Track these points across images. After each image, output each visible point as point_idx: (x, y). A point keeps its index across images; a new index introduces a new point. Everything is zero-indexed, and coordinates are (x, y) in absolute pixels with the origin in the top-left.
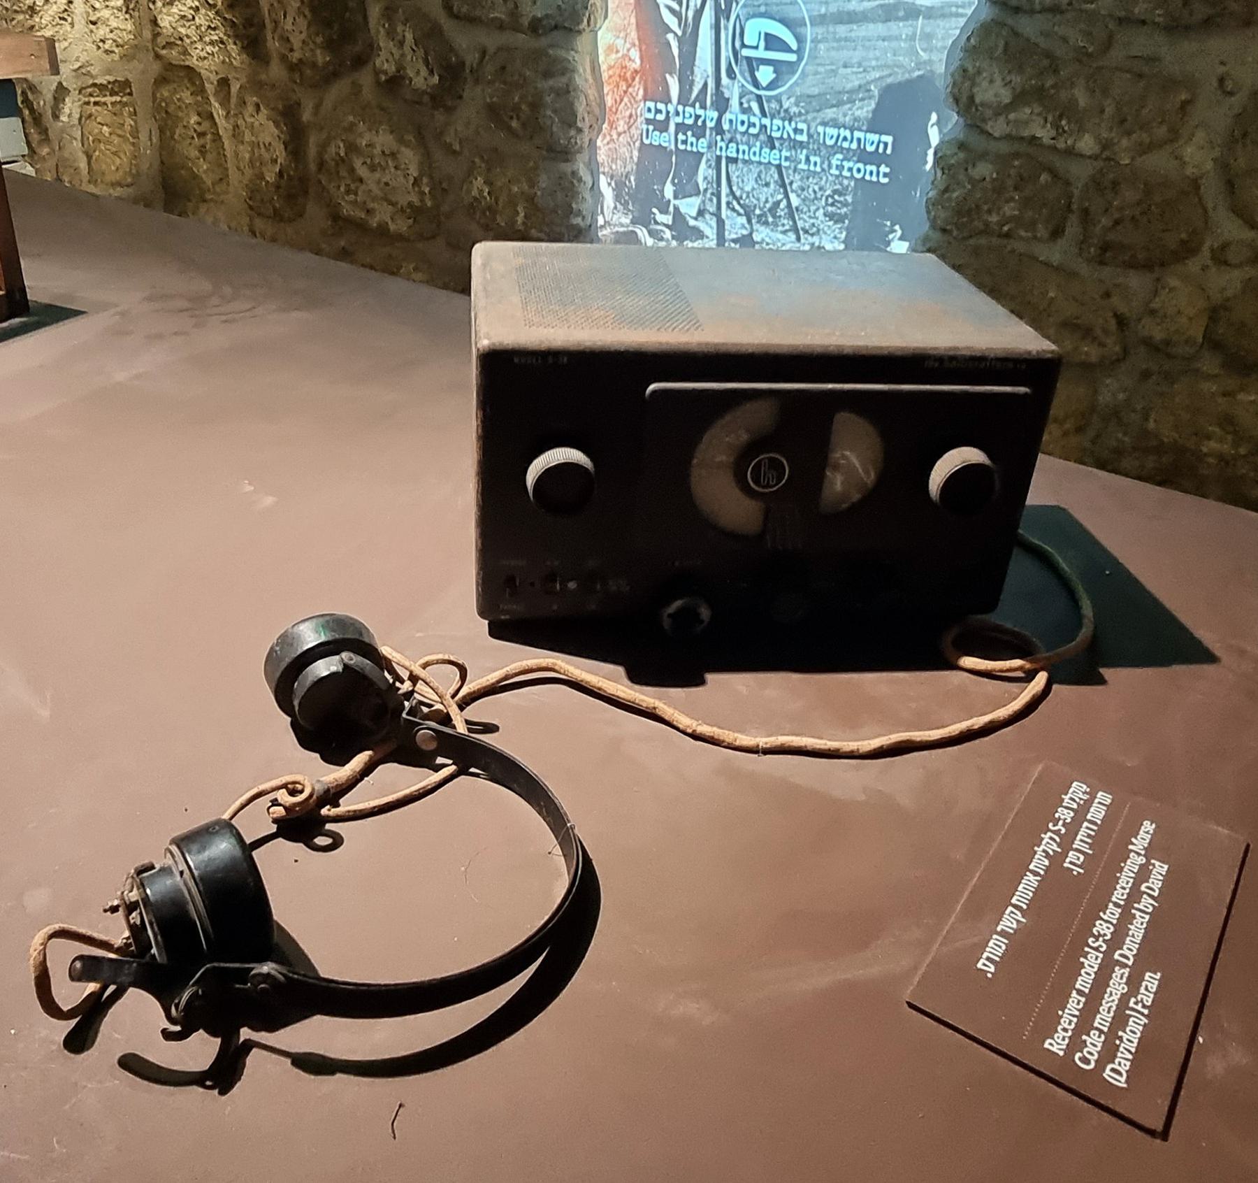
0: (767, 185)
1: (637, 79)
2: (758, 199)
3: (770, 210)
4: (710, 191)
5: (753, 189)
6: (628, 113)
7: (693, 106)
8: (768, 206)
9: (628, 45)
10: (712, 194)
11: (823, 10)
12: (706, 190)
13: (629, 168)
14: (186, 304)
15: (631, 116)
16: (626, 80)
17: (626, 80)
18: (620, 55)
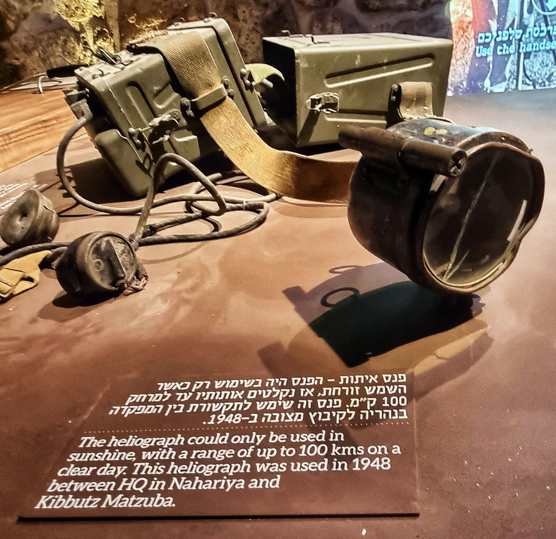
0: (547, 66)
1: (470, 27)
2: (541, 75)
3: (547, 79)
4: (512, 77)
5: (539, 69)
6: (463, 47)
7: (508, 30)
8: (546, 77)
9: (465, 8)
10: (514, 79)
11: (535, 502)
12: (510, 78)
13: (462, 78)
14: (81, 333)
15: (465, 48)
16: (463, 29)
17: (463, 29)
18: (459, 15)
